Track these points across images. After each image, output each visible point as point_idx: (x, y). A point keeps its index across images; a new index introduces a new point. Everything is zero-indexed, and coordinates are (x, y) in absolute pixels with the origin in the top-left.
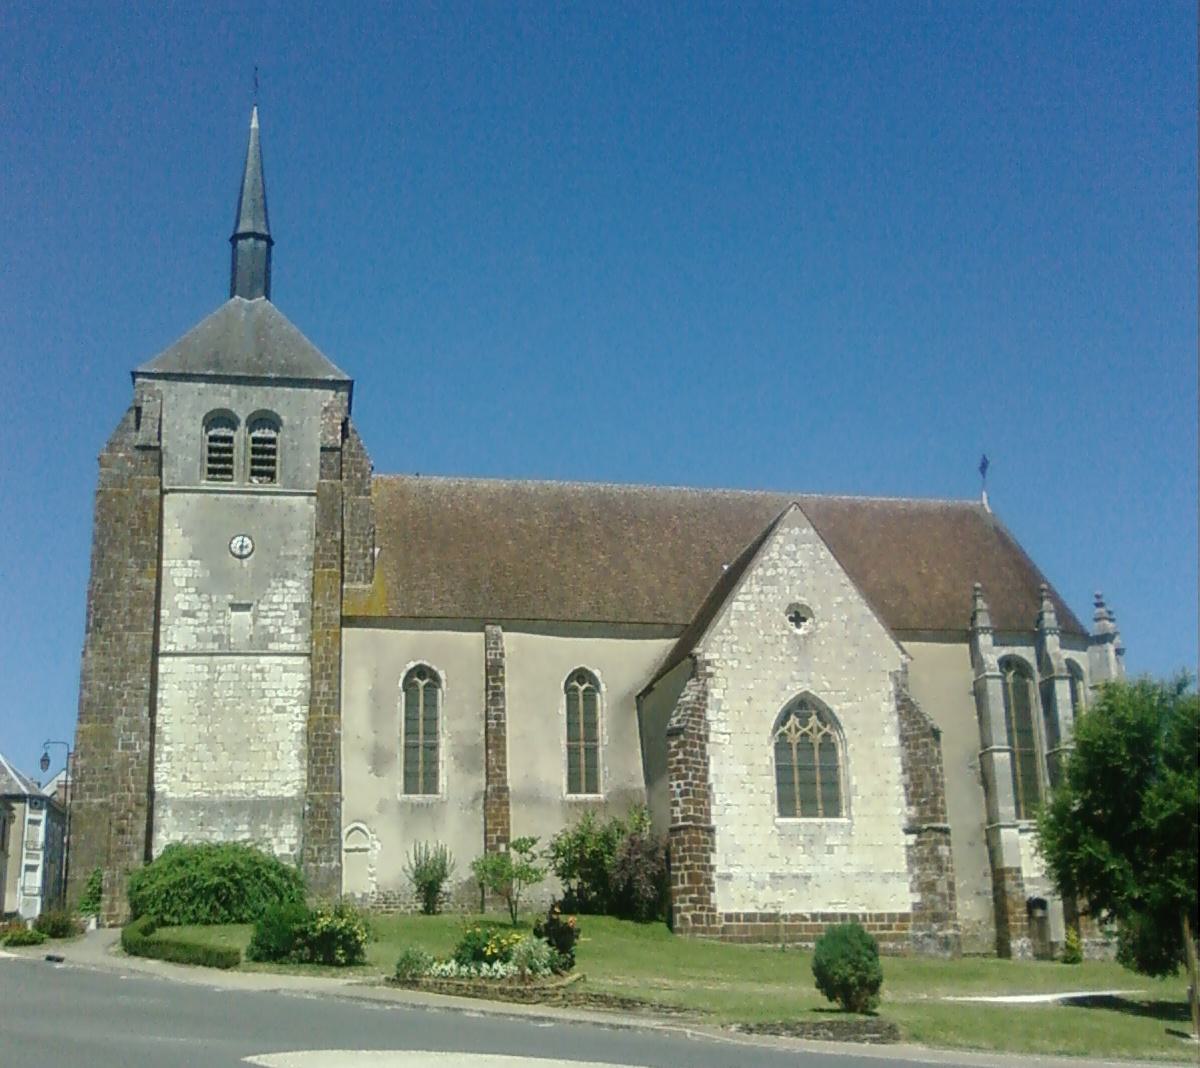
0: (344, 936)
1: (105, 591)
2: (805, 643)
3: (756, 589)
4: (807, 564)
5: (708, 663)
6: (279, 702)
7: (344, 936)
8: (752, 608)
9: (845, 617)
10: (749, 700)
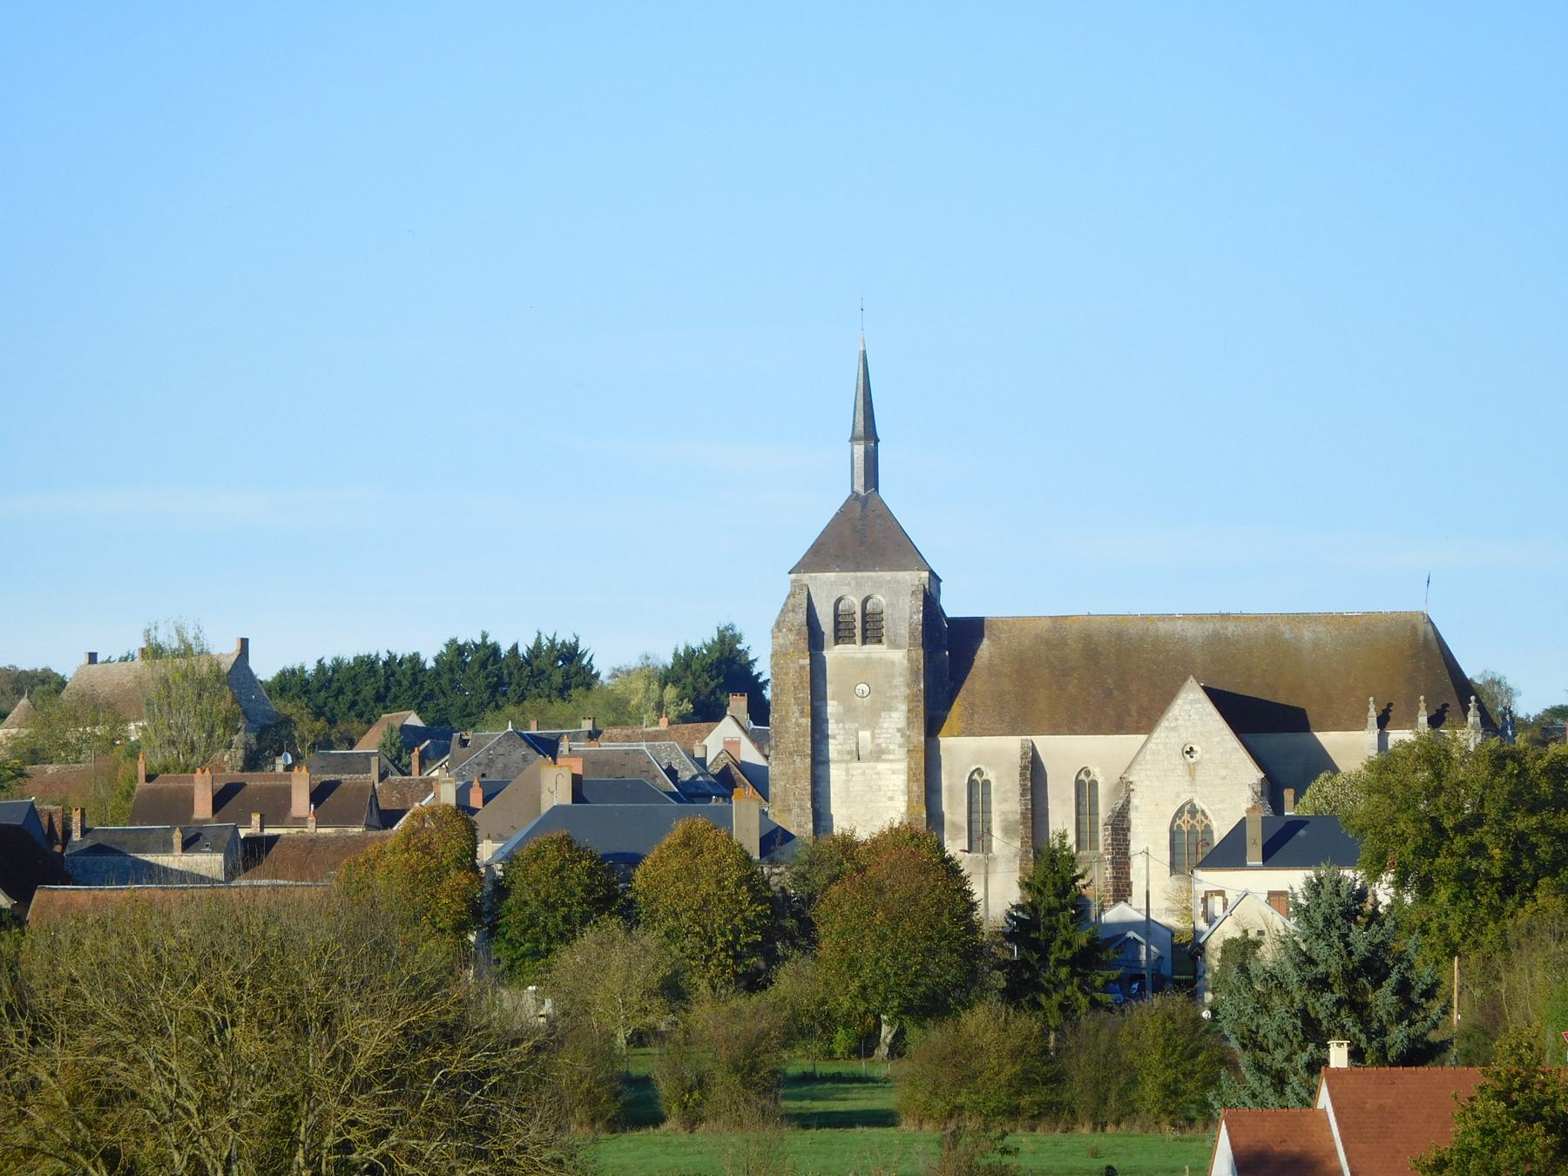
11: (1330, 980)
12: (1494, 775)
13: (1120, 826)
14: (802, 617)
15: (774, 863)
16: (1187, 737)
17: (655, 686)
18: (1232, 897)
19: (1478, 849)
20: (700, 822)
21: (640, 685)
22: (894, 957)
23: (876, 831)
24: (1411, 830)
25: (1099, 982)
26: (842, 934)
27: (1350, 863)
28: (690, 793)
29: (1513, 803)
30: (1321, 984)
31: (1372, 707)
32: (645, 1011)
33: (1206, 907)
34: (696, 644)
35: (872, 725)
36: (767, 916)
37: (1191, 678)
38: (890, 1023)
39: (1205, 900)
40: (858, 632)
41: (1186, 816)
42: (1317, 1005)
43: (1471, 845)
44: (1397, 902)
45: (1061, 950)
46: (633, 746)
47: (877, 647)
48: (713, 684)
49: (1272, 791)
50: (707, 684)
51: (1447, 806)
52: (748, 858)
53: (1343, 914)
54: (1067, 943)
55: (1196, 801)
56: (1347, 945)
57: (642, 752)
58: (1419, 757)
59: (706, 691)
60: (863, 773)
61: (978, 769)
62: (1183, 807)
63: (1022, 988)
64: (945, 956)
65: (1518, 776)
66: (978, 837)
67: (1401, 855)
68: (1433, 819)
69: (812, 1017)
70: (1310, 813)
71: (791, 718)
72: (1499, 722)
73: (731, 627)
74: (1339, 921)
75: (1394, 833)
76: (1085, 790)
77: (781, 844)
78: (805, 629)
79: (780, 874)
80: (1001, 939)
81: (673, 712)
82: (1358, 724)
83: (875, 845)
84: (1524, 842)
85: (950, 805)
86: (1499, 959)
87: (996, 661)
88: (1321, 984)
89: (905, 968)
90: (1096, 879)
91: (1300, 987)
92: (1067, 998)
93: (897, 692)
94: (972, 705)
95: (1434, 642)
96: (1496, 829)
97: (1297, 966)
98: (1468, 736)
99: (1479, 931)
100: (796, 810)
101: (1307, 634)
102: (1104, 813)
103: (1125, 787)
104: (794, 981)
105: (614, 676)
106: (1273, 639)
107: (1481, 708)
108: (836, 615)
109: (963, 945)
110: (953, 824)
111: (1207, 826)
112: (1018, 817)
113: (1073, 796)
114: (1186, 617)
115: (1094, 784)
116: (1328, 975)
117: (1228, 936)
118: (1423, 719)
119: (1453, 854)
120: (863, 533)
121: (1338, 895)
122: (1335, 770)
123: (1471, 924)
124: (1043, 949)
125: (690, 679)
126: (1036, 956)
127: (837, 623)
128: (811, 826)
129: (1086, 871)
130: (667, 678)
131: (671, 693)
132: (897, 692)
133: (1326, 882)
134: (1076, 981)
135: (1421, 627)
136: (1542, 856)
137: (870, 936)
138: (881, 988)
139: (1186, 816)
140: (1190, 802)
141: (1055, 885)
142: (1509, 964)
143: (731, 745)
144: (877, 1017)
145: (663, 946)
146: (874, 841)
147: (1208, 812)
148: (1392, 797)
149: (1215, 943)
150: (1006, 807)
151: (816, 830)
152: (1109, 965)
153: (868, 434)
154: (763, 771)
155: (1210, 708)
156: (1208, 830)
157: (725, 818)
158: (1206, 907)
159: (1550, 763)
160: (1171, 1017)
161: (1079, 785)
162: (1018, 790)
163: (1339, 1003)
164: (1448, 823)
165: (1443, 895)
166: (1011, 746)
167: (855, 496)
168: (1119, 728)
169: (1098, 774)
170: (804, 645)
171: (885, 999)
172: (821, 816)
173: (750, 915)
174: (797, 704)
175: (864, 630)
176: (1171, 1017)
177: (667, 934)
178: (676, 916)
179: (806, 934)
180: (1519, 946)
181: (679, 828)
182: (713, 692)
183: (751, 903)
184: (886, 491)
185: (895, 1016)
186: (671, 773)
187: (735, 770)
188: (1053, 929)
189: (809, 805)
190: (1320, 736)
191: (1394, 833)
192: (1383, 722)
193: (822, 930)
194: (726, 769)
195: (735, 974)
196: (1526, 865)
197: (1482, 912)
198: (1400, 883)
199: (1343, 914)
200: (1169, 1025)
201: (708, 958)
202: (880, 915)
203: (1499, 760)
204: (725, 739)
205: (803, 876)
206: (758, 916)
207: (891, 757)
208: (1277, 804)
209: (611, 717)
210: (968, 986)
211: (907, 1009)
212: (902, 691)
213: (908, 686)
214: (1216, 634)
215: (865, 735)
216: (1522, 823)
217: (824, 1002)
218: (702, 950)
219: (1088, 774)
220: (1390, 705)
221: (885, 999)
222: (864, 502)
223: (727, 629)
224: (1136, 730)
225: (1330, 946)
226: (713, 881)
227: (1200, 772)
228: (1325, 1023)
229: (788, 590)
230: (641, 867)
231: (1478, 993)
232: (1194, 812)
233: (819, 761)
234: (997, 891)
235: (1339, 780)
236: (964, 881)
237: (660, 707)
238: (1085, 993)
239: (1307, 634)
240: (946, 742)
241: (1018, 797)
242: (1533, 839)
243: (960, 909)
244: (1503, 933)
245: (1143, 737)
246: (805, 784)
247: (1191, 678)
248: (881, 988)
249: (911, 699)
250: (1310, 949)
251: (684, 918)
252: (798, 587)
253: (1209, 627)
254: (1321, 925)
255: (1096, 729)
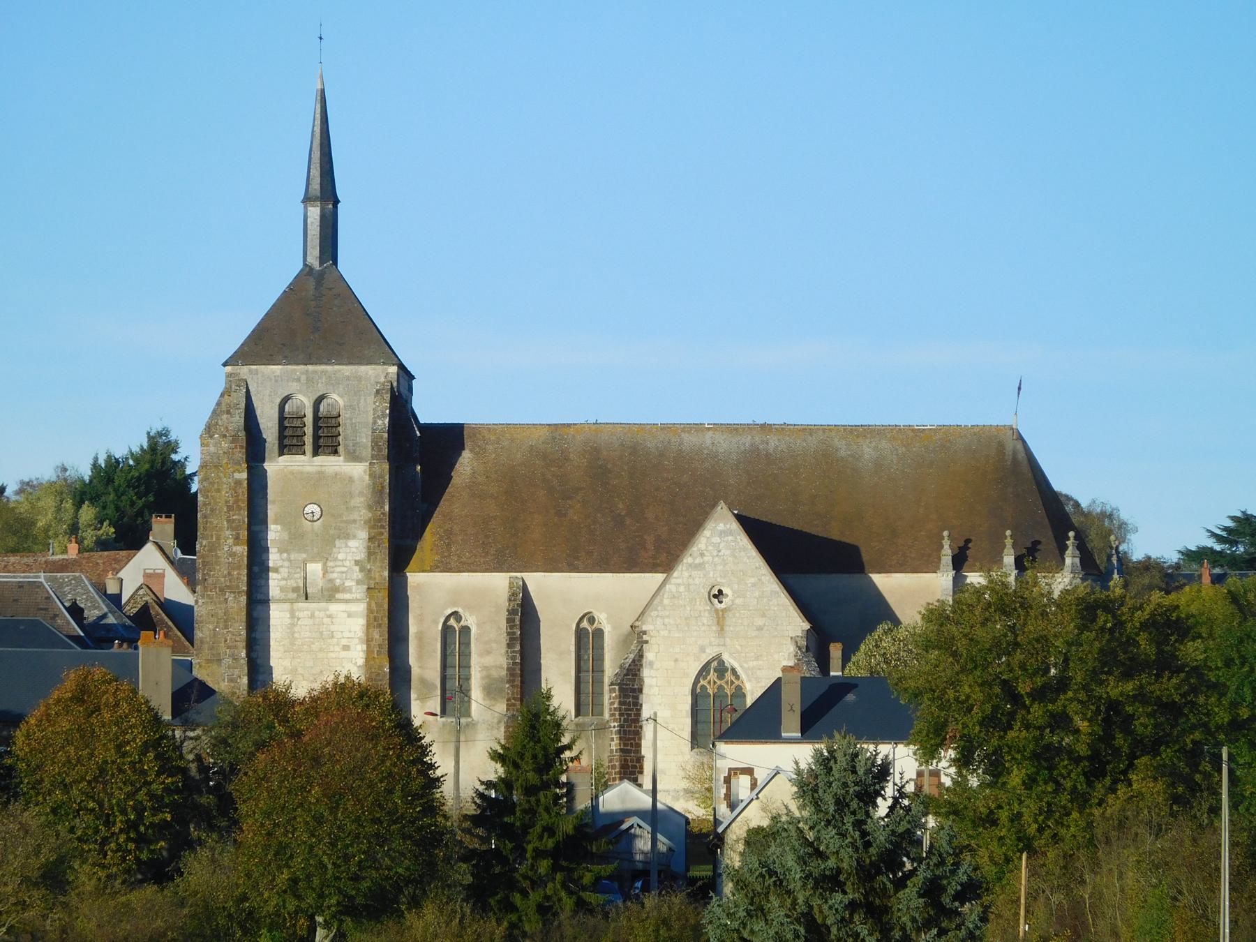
0: (127, 833)
1: (210, 551)
2: (723, 617)
3: (686, 574)
4: (728, 552)
5: (645, 633)
6: (344, 642)
7: (127, 833)
8: (682, 589)
9: (757, 594)
10: (676, 660)
11: (842, 878)
12: (1082, 628)
13: (630, 686)
14: (238, 419)
15: (188, 725)
16: (714, 576)
17: (68, 505)
18: (761, 776)
19: (1060, 721)
20: (98, 673)
21: (49, 503)
22: (333, 844)
23: (317, 686)
24: (978, 695)
25: (588, 878)
26: (268, 815)
27: (897, 735)
28: (97, 636)
29: (1104, 664)
30: (830, 882)
31: (946, 544)
32: (24, 906)
33: (729, 789)
34: (120, 452)
35: (325, 556)
36: (177, 791)
37: (722, 504)
38: (327, 925)
39: (727, 781)
40: (308, 439)
41: (712, 676)
42: (825, 907)
43: (1052, 715)
44: (960, 784)
45: (541, 838)
46: (29, 577)
47: (332, 458)
48: (140, 503)
49: (817, 645)
50: (133, 504)
51: (1023, 666)
52: (156, 719)
53: (859, 796)
54: (550, 830)
55: (725, 657)
56: (864, 834)
57: (40, 585)
58: (989, 604)
59: (131, 511)
60: (312, 616)
61: (455, 614)
62: (708, 664)
63: (491, 886)
64: (398, 844)
65: (1111, 631)
66: (453, 697)
67: (965, 726)
68: (1005, 682)
69: (230, 916)
70: (864, 673)
71: (223, 541)
72: (1100, 561)
73: (164, 433)
74: (854, 804)
75: (957, 699)
76: (587, 641)
77: (198, 701)
78: (242, 434)
79: (197, 738)
80: (467, 824)
81: (90, 537)
82: (929, 564)
83: (315, 704)
84: (1118, 713)
85: (420, 657)
86: (1083, 858)
87: (481, 479)
88: (830, 882)
89: (347, 858)
90: (587, 754)
91: (804, 886)
92: (547, 898)
93: (355, 516)
94: (449, 533)
95: (1025, 462)
96: (1082, 695)
97: (802, 861)
98: (1062, 580)
99: (1059, 823)
100: (227, 661)
101: (868, 451)
102: (610, 669)
103: (637, 638)
104: (207, 871)
105: (20, 491)
106: (825, 457)
107: (1082, 547)
108: (282, 418)
109: (420, 829)
110: (423, 681)
111: (739, 688)
112: (504, 673)
113: (573, 648)
114: (718, 427)
115: (599, 633)
116: (839, 871)
117: (754, 824)
118: (1009, 560)
119: (1027, 726)
120: (318, 317)
121: (854, 772)
122: (896, 622)
123: (1050, 812)
124: (516, 836)
125: (112, 496)
126: (509, 845)
127: (282, 428)
128: (245, 680)
129: (573, 741)
130: (83, 493)
131: (87, 513)
132: (355, 516)
133: (839, 755)
134: (559, 876)
135: (1010, 445)
136: (1140, 730)
137: (301, 817)
138: (316, 881)
139: (712, 676)
140: (718, 658)
141: (535, 757)
142: (1095, 865)
143: (152, 580)
144: (311, 918)
145: (49, 824)
146: (314, 700)
147: (740, 671)
148: (955, 654)
149: (736, 834)
150: (489, 660)
151: (252, 685)
152: (603, 858)
153: (325, 192)
154: (190, 609)
155: (744, 541)
156: (739, 693)
157: (129, 669)
158: (729, 789)
159: (1152, 615)
160: (665, 922)
161: (580, 634)
162: (504, 639)
163: (852, 906)
164: (1024, 688)
165: (1016, 778)
166: (498, 583)
167: (307, 271)
168: (631, 564)
169: (604, 620)
170: (240, 455)
171: (321, 896)
172: (258, 667)
173: (157, 788)
174: (230, 527)
175: (316, 438)
176: (665, 922)
177: (54, 811)
178: (66, 788)
179: (223, 814)
180: (1108, 841)
181: (70, 680)
182: (140, 513)
183: (158, 774)
184: (347, 265)
185: (334, 917)
186: (76, 611)
187: (156, 610)
188: (532, 812)
189: (243, 654)
190: (878, 579)
191: (957, 699)
192: (959, 562)
193: (243, 808)
194: (145, 608)
195: (138, 860)
196: (1120, 740)
197: (1064, 798)
198: (963, 762)
199: (859, 796)
200: (663, 932)
201: (105, 841)
202: (316, 791)
203: (1088, 610)
204: (146, 570)
205: (224, 741)
206: (167, 789)
207: (347, 596)
208: (823, 662)
209: (11, 541)
210: (425, 878)
211: (349, 909)
212: (362, 514)
213: (370, 508)
214: (754, 451)
215: (315, 568)
216: (1115, 688)
217: (244, 898)
218: (97, 831)
219: (592, 620)
220: (968, 541)
221: (321, 896)
222: (320, 277)
223: (160, 434)
224: (653, 568)
225: (843, 835)
226: (111, 746)
227: (730, 621)
228: (834, 930)
229: (221, 386)
230: (23, 727)
231: (1057, 898)
232: (722, 669)
233: (257, 601)
234: (465, 764)
235: (901, 633)
236: (424, 750)
237: (74, 529)
238: (571, 893)
239: (868, 451)
240: (414, 578)
241: (503, 649)
242: (1129, 709)
243: (415, 786)
244: (1090, 825)
245: (660, 577)
246: (240, 628)
247: (722, 504)
248: (316, 881)
249: (372, 524)
250: (818, 838)
251: (75, 792)
252: (233, 384)
253: (747, 440)
254: (832, 809)
255: (603, 565)
